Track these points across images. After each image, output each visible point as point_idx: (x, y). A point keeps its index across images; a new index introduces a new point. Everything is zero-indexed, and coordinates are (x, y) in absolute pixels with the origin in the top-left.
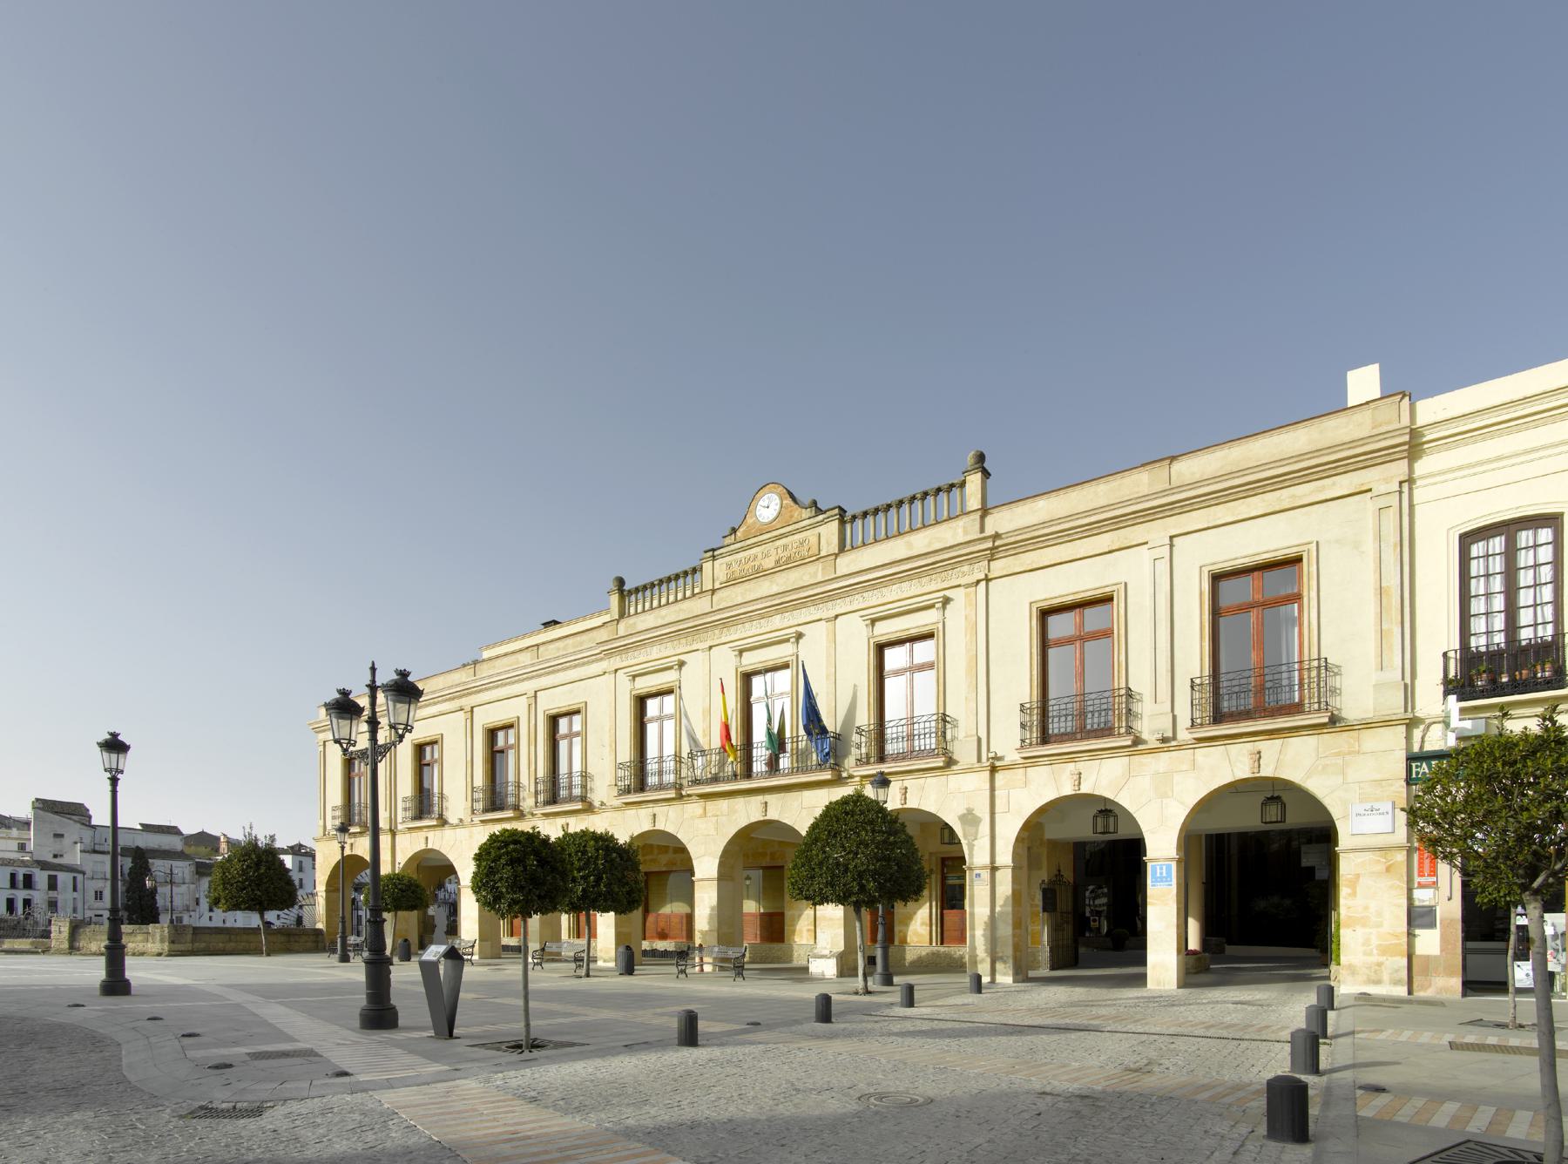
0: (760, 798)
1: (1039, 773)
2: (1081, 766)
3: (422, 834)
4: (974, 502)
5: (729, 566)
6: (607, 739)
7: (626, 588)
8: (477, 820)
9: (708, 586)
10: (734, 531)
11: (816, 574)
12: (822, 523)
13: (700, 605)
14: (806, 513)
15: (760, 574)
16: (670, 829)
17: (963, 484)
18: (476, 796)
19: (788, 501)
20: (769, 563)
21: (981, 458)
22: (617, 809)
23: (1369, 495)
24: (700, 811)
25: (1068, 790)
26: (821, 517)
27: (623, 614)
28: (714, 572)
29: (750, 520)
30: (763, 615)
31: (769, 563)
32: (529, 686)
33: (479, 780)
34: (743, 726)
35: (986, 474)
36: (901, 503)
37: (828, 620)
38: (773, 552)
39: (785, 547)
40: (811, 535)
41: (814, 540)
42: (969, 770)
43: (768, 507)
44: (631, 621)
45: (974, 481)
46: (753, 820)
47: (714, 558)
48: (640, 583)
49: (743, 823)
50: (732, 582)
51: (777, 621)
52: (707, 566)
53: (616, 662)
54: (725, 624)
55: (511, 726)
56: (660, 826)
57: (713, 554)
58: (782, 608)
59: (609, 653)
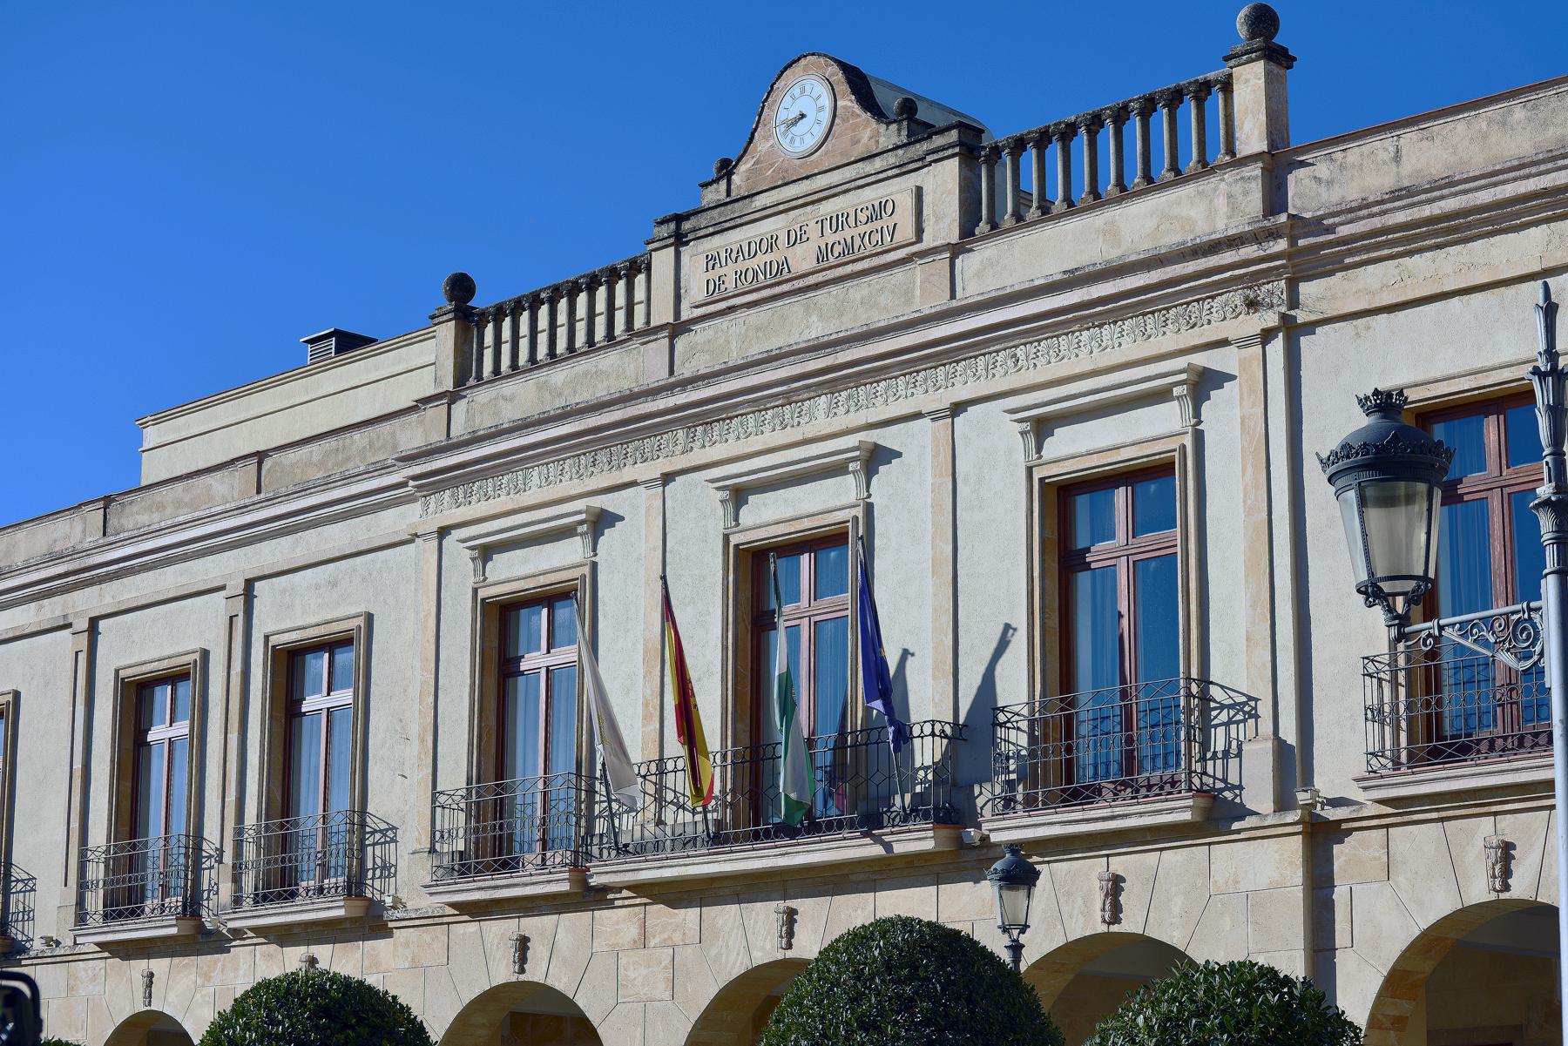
0: (140, 966)
1: (1417, 842)
2: (1120, 864)
3: (500, 931)
4: (1252, 136)
5: (712, 261)
6: (418, 723)
7: (479, 302)
8: (88, 942)
9: (663, 314)
10: (727, 169)
11: (908, 295)
12: (922, 162)
13: (641, 364)
14: (890, 135)
15: (782, 287)
16: (561, 982)
17: (1227, 86)
18: (444, 821)
19: (848, 102)
20: (802, 259)
21: (1264, 21)
22: (429, 921)
23: (223, 594)
24: (631, 931)
25: (1480, 891)
26: (925, 146)
27: (466, 373)
28: (680, 277)
29: (761, 146)
30: (792, 393)
31: (802, 259)
32: (232, 567)
33: (456, 773)
34: (508, 742)
35: (1278, 57)
36: (1121, 116)
37: (935, 416)
38: (813, 230)
39: (838, 222)
40: (899, 191)
41: (906, 203)
42: (1262, 834)
43: (807, 105)
44: (482, 396)
45: (1250, 81)
46: (760, 958)
47: (680, 240)
48: (507, 295)
49: (735, 966)
50: (721, 307)
51: (820, 416)
52: (662, 261)
53: (445, 508)
54: (703, 417)
55: (345, 641)
56: (535, 973)
57: (680, 231)
58: (833, 382)
59: (431, 484)
